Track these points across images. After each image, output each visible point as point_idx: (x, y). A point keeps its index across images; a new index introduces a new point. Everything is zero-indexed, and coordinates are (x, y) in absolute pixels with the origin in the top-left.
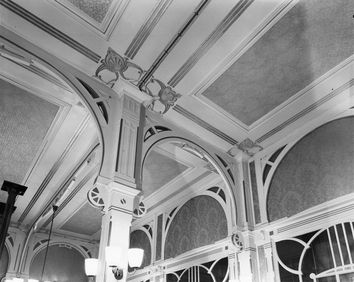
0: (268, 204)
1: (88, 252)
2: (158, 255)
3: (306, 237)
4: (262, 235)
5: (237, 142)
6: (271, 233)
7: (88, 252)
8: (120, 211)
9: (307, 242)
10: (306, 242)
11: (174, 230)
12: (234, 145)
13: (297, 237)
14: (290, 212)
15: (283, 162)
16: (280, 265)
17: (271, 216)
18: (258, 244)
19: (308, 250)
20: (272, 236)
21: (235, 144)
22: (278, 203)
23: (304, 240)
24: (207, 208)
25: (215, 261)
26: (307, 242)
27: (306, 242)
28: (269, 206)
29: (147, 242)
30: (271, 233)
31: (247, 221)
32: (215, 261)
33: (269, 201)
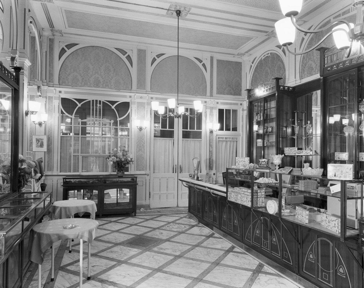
0: (60, 73)
1: (202, 63)
2: (272, 76)
3: (80, 101)
4: (54, 91)
5: (54, 28)
6: (60, 92)
7: (202, 63)
8: (10, 31)
9: (80, 103)
10: (80, 103)
11: (265, 71)
12: (50, 28)
13: (75, 99)
14: (74, 84)
15: (74, 53)
16: (62, 110)
17: (61, 81)
18: (49, 95)
19: (79, 107)
20: (60, 94)
21: (52, 28)
22: (67, 76)
23: (79, 102)
24: (315, 72)
25: (87, 100)
26: (80, 103)
27: (80, 103)
28: (61, 75)
29: (264, 71)
30: (60, 92)
31: (46, 79)
32: (87, 100)
33: (61, 72)
